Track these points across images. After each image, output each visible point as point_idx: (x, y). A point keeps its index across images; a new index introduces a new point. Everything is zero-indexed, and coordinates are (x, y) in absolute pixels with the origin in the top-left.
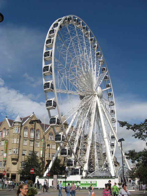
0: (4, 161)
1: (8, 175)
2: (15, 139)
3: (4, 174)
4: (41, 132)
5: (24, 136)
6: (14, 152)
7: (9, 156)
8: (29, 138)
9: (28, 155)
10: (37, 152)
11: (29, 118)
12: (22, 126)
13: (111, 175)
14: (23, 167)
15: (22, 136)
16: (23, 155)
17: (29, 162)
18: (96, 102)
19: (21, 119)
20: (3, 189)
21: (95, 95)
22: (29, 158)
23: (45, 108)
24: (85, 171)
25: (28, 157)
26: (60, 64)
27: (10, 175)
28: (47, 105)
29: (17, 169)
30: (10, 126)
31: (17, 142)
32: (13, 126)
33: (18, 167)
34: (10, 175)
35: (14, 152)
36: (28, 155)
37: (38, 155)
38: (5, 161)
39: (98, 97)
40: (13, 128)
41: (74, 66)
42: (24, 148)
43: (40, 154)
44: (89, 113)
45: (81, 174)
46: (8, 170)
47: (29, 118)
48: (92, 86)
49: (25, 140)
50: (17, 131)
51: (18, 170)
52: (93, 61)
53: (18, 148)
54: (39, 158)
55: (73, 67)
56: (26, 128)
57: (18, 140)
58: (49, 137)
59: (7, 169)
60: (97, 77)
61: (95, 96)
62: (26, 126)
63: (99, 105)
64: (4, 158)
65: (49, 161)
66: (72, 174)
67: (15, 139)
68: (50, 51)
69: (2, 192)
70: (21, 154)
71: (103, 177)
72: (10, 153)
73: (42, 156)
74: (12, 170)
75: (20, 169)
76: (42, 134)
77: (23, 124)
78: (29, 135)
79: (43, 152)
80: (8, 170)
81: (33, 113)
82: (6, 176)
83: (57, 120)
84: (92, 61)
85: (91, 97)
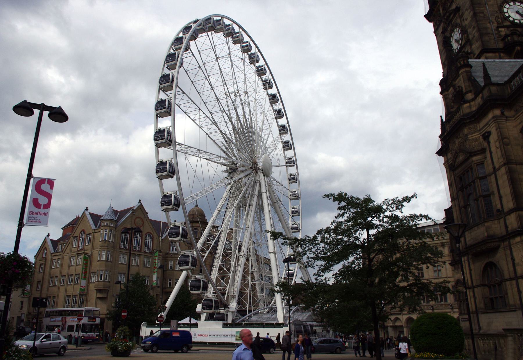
4: (155, 238)
11: (131, 212)
29: (108, 310)
30: (93, 227)
32: (100, 226)
39: (262, 174)
40: (99, 230)
56: (149, 235)
66: (209, 318)
67: (104, 253)
69: (74, 352)
72: (93, 279)
75: (113, 309)
78: (425, 355)
81: (140, 200)
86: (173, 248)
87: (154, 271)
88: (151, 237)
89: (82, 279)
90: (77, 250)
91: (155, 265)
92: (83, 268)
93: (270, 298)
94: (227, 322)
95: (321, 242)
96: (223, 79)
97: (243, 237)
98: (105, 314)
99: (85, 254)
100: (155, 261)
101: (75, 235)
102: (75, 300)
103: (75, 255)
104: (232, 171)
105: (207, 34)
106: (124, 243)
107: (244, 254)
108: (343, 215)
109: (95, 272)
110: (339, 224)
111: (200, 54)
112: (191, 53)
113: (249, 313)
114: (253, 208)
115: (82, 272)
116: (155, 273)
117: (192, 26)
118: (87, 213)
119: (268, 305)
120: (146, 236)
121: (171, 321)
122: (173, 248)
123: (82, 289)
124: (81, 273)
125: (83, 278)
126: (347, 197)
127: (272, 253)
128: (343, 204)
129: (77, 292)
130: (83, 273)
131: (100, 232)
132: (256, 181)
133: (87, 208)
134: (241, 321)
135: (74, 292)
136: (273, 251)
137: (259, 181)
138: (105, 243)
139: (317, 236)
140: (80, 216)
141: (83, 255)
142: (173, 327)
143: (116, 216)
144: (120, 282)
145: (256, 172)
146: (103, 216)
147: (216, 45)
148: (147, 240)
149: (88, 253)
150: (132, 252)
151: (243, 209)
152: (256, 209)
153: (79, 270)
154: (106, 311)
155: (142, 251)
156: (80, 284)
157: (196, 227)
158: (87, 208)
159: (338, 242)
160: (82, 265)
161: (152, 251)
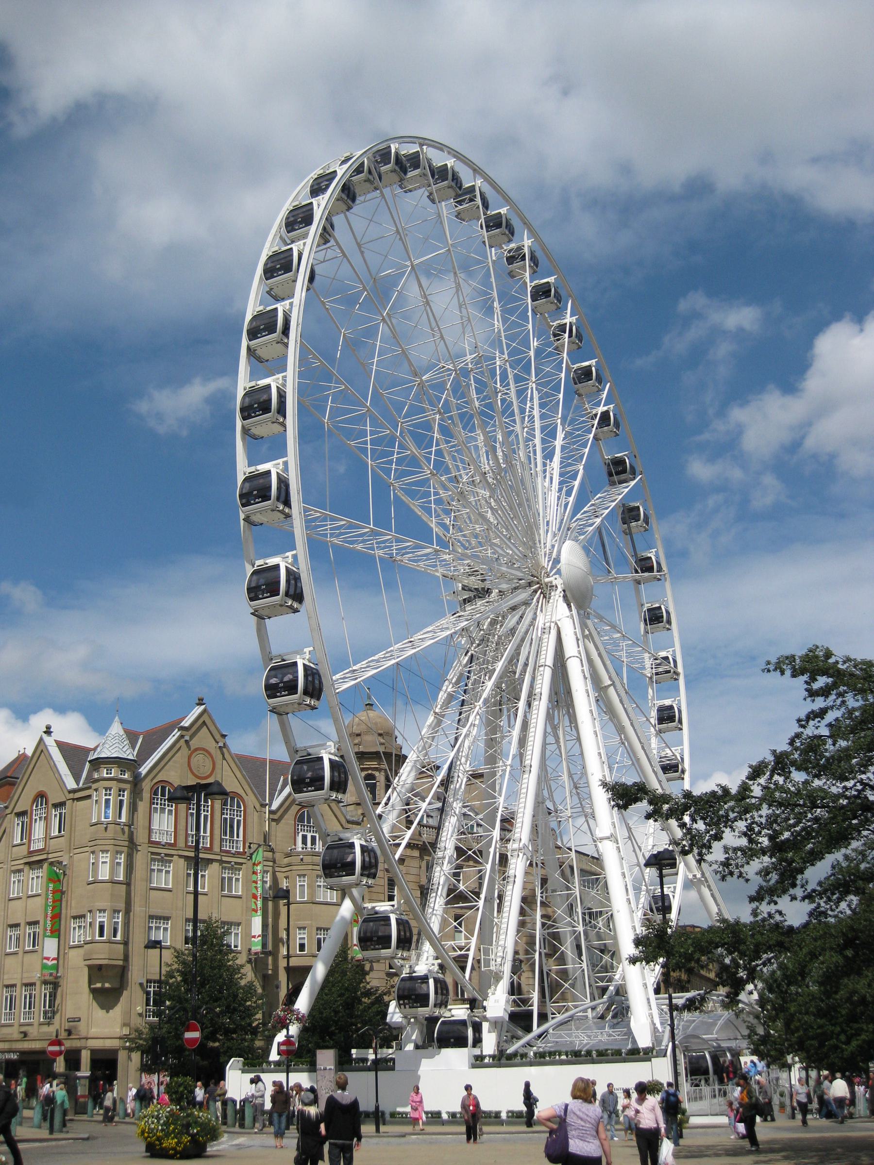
0: (45, 983)
1: (73, 1060)
2: (105, 858)
3: (52, 1053)
4: (250, 809)
5: (155, 838)
6: (102, 928)
7: (72, 953)
8: (181, 843)
9: (180, 945)
10: (231, 924)
11: (176, 734)
12: (136, 782)
13: (634, 1041)
14: (156, 1014)
15: (141, 837)
16: (155, 944)
17: (185, 980)
18: (554, 632)
19: (132, 737)
20: (52, 1131)
21: (546, 591)
22: (184, 963)
23: (244, 606)
24: (496, 1024)
25: (178, 954)
26: (338, 382)
27: (85, 1057)
28: (254, 593)
29: (125, 1025)
31: (113, 871)
32: (90, 780)
33: (128, 1013)
34: (85, 1057)
35: (102, 928)
36: (180, 945)
37: (234, 940)
38: (51, 979)
41: (423, 410)
42: (159, 904)
43: (248, 936)
44: (509, 671)
45: (478, 1041)
46: (69, 1032)
47: (176, 734)
48: (531, 530)
49: (162, 860)
50: (111, 811)
51: (126, 1031)
52: (543, 429)
53: (122, 906)
54: (242, 960)
55: (418, 419)
56: (163, 788)
57: (122, 859)
58: (299, 839)
59: (67, 1025)
60: (569, 494)
61: (546, 597)
62: (160, 778)
63: (571, 648)
64: (44, 966)
65: (298, 975)
67: (105, 858)
68: (281, 307)
69: (48, 1147)
70: (138, 941)
71: (589, 1053)
72: (76, 936)
73: (257, 948)
74: (94, 1031)
76: (253, 818)
77: (144, 770)
79: (265, 926)
80: (69, 1032)
82: (60, 1066)
83: (306, 676)
84: (537, 433)
85: (523, 596)
86: (304, 838)
87: (254, 907)
88: (239, 806)
89: (45, 936)
90: (26, 853)
91: (256, 888)
92: (46, 905)
93: (602, 979)
94: (482, 1051)
95: (762, 800)
96: (434, 324)
97: (514, 794)
98: (120, 1038)
99: (52, 864)
100: (254, 877)
101: (17, 810)
102: (30, 997)
103: (21, 867)
104: (472, 594)
105: (382, 192)
106: (232, 835)
107: (521, 845)
108: (821, 713)
109: (84, 916)
110: (814, 745)
111: (362, 253)
112: (336, 248)
113: (538, 1026)
114: (541, 707)
115: (46, 916)
116: (256, 911)
117: (335, 172)
118: (49, 741)
119: (597, 997)
120: (156, 793)
121: (423, 1060)
122: (304, 838)
123: (46, 964)
124: (40, 918)
125: (48, 933)
126: (831, 661)
127: (607, 838)
128: (822, 681)
129: (36, 976)
130: (49, 919)
131: (89, 797)
132: (548, 625)
133: (48, 727)
134: (524, 1046)
135: (25, 975)
136: (608, 835)
137: (556, 624)
138: (106, 829)
139: (751, 782)
140: (29, 753)
141: (45, 866)
142: (325, 1069)
143: (134, 748)
144: (159, 942)
145: (545, 597)
146: (95, 749)
147: (378, 200)
148: (228, 817)
149: (60, 859)
150: (201, 855)
151: (508, 710)
152: (548, 709)
153: (37, 909)
154: (121, 1029)
155: (216, 849)
156: (40, 951)
157: (370, 772)
158: (48, 727)
159: (813, 799)
160: (44, 895)
161: (244, 848)
